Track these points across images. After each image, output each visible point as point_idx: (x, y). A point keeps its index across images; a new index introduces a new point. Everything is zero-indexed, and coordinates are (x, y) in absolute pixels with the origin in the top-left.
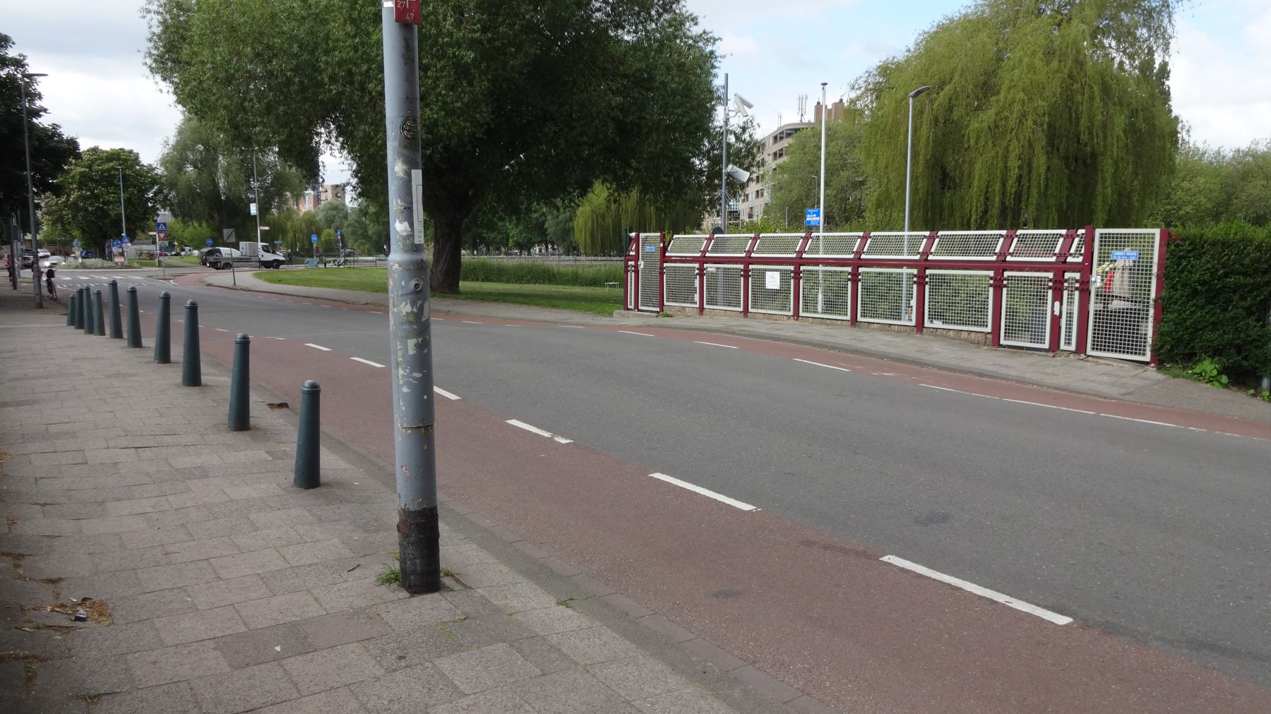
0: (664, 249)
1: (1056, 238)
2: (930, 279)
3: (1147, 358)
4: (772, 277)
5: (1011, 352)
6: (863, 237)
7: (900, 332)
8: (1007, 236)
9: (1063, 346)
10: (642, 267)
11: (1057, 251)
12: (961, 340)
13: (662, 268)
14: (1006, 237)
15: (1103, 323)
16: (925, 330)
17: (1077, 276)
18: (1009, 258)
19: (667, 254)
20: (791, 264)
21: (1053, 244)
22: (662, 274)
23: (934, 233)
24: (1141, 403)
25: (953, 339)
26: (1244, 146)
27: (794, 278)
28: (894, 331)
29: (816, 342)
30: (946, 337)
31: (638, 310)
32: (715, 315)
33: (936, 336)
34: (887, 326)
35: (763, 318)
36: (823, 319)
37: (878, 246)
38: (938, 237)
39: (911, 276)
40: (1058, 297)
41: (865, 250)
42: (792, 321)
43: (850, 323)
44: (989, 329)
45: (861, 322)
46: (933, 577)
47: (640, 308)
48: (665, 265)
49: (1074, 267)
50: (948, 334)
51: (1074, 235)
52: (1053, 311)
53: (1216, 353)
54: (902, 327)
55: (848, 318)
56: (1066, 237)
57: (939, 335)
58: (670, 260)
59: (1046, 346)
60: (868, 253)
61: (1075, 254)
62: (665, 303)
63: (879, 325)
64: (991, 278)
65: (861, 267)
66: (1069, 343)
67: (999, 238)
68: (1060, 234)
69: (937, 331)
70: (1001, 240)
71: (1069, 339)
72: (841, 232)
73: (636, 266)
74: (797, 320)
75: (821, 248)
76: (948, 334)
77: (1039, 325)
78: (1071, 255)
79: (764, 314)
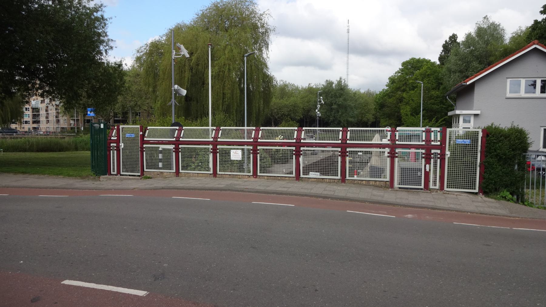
0: (143, 136)
1: (174, 130)
2: (182, 149)
3: (477, 191)
4: (235, 153)
5: (406, 191)
6: (179, 129)
7: (330, 182)
8: (217, 129)
9: (431, 186)
10: (123, 147)
11: (175, 136)
12: (371, 185)
13: (142, 148)
14: (178, 130)
15: (324, 170)
16: (347, 181)
17: (115, 145)
18: (181, 139)
19: (145, 139)
20: (422, 149)
21: (173, 134)
22: (142, 152)
23: (258, 128)
24: (522, 218)
25: (365, 185)
26: (381, 90)
27: (296, 155)
28: (326, 182)
29: (199, 188)
30: (361, 184)
31: (121, 175)
32: (190, 176)
33: (354, 184)
34: (321, 179)
35: (229, 178)
36: (275, 176)
37: (189, 134)
38: (221, 130)
39: (248, 150)
40: (428, 162)
41: (182, 136)
42: (252, 179)
43: (295, 178)
44: (174, 171)
45: (303, 178)
46: (127, 289)
47: (122, 173)
48: (145, 146)
49: (436, 147)
50: (362, 183)
51: (182, 129)
52: (425, 169)
53: (506, 186)
54: (332, 180)
55: (339, 177)
56: (256, 130)
57: (356, 183)
58: (148, 142)
59: (422, 187)
60: (183, 138)
61: (261, 138)
62: (145, 170)
63: (315, 179)
64: (340, 152)
65: (112, 143)
66: (114, 171)
67: (176, 130)
68: (176, 129)
69: (354, 181)
70: (177, 131)
71: (114, 170)
72: (154, 126)
73: (118, 147)
74: (256, 178)
75: (246, 137)
76: (362, 183)
77: (134, 165)
78: (181, 137)
79: (230, 175)
